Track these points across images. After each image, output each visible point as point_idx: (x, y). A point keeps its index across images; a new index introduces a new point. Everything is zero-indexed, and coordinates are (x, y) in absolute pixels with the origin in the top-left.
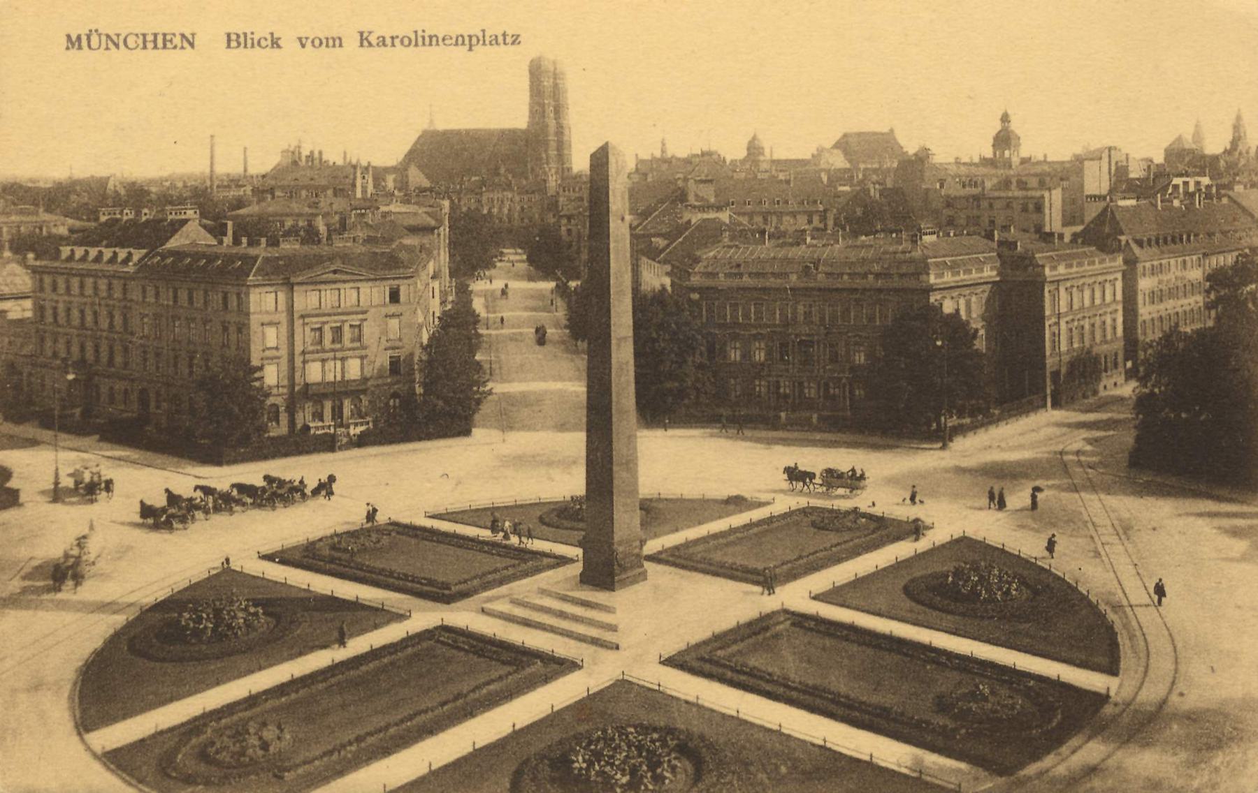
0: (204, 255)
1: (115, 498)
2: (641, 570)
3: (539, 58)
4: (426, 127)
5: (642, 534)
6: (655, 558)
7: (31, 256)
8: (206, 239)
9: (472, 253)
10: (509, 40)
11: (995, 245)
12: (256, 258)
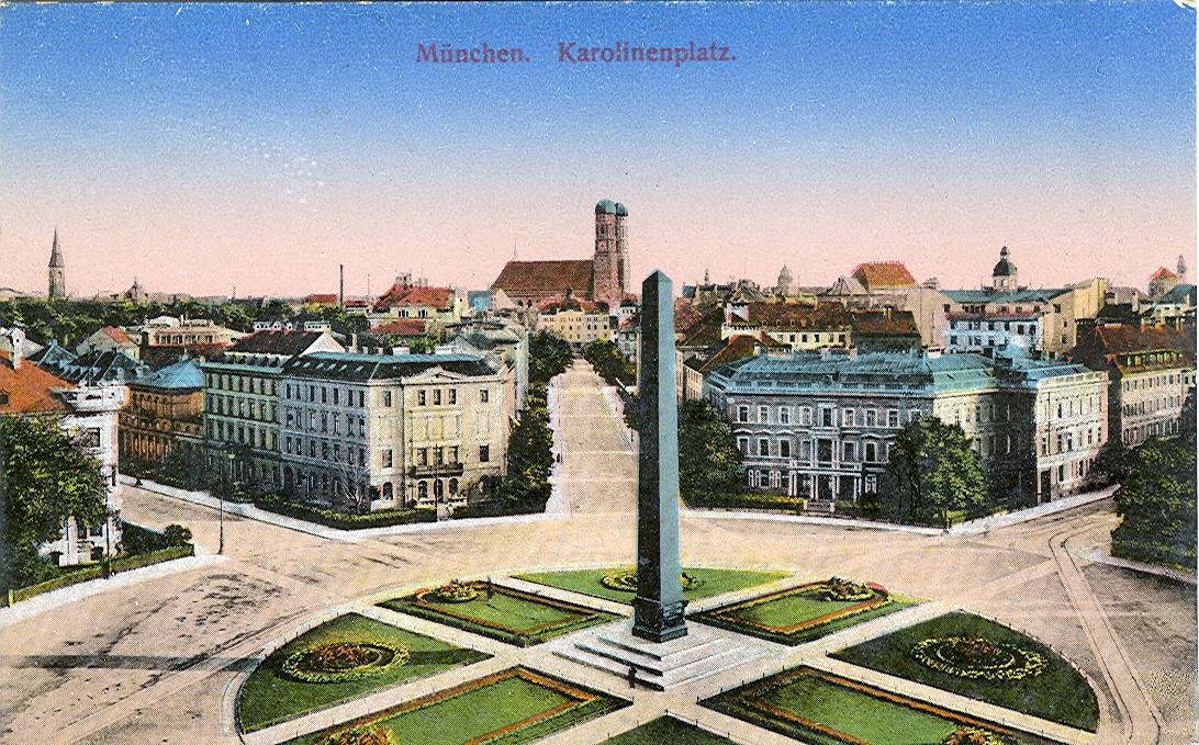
0: (331, 361)
1: (280, 585)
2: (682, 627)
3: (604, 202)
4: (510, 259)
5: (684, 597)
6: (697, 617)
7: (202, 359)
8: (337, 349)
9: (549, 357)
10: (718, 54)
11: (992, 361)
12: (375, 363)
